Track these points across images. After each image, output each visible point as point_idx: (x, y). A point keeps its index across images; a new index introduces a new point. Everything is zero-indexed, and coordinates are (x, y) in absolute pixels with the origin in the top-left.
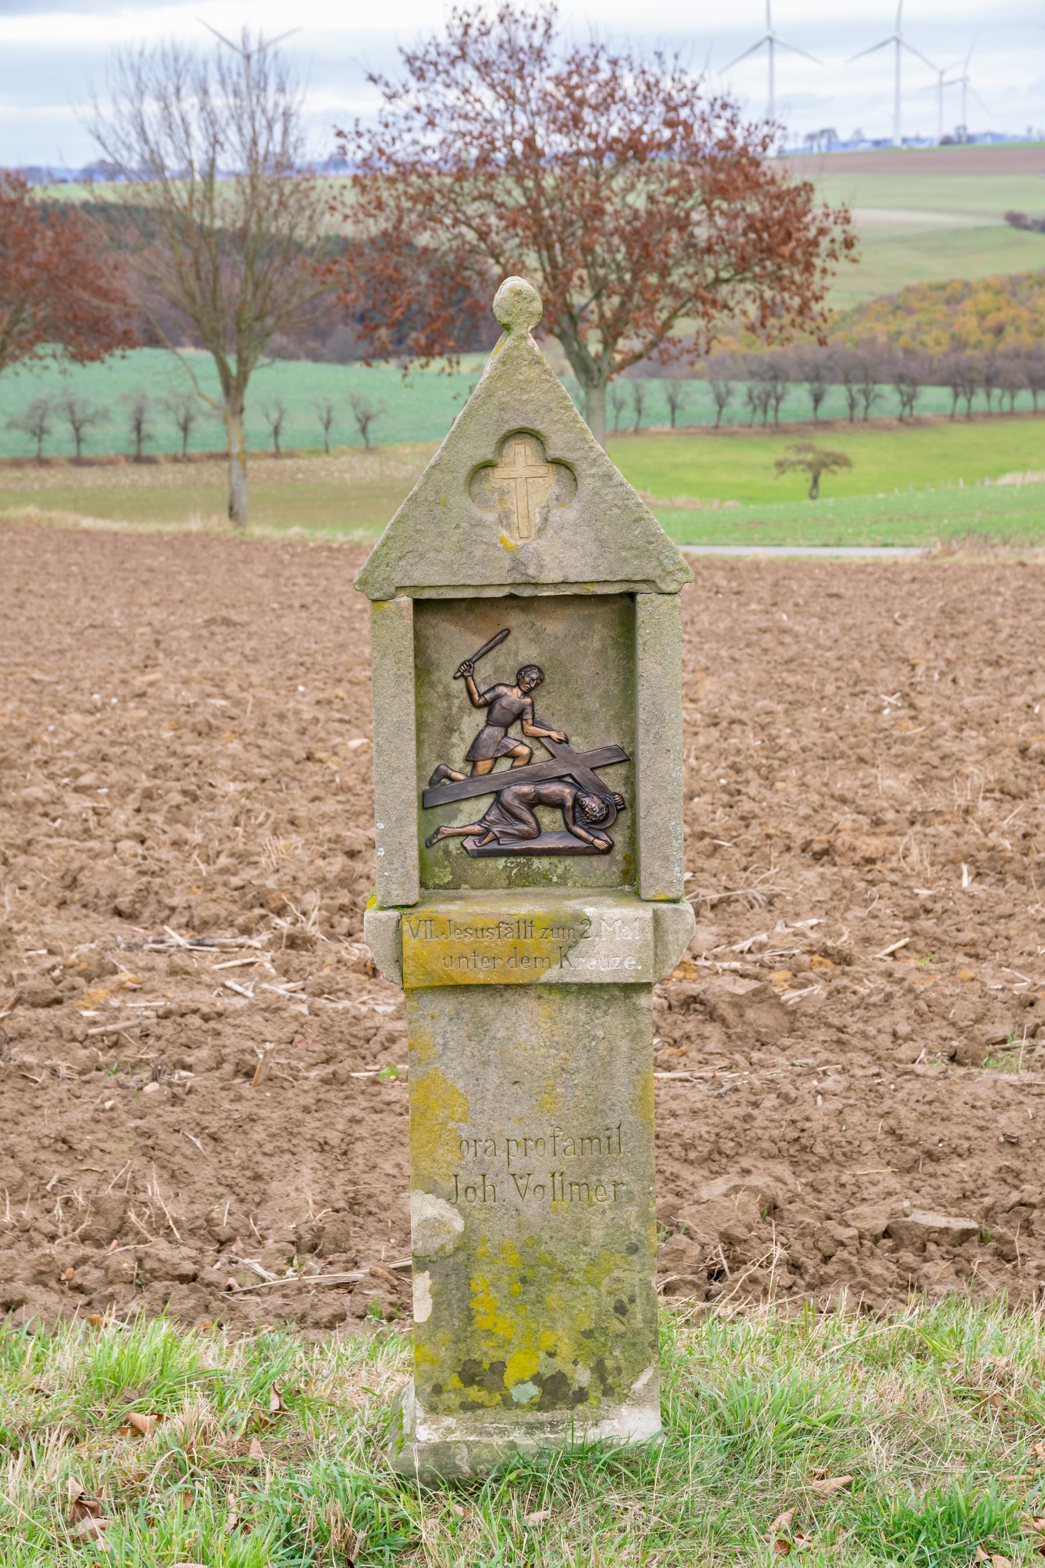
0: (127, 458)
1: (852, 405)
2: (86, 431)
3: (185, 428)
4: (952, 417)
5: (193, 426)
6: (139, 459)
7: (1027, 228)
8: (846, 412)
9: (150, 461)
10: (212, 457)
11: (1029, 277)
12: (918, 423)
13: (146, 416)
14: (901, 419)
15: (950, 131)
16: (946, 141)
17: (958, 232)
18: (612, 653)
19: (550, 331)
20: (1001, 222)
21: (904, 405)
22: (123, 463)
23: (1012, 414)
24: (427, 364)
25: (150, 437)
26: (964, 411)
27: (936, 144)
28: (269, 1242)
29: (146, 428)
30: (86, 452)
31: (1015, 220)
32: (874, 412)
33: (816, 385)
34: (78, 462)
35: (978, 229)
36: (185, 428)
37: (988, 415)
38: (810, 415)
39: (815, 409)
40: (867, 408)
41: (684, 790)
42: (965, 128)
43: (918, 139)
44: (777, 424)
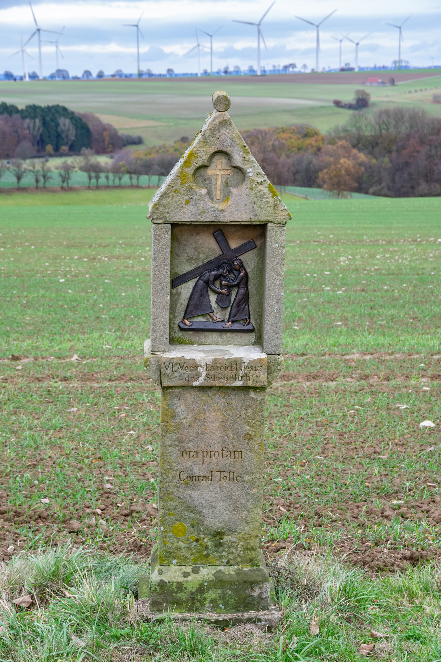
1: (37, 181)
4: (89, 188)
7: (342, 107)
8: (34, 184)
12: (71, 189)
14: (62, 188)
15: (343, 65)
16: (342, 70)
17: (312, 108)
20: (332, 104)
21: (63, 182)
23: (120, 187)
26: (95, 185)
27: (338, 70)
28: (5, 474)
31: (337, 104)
32: (47, 185)
33: (107, 174)
35: (321, 107)
37: (107, 187)
38: (16, 185)
39: (18, 183)
40: (45, 183)
42: (349, 64)
43: (187, 74)
44: (44, 187)
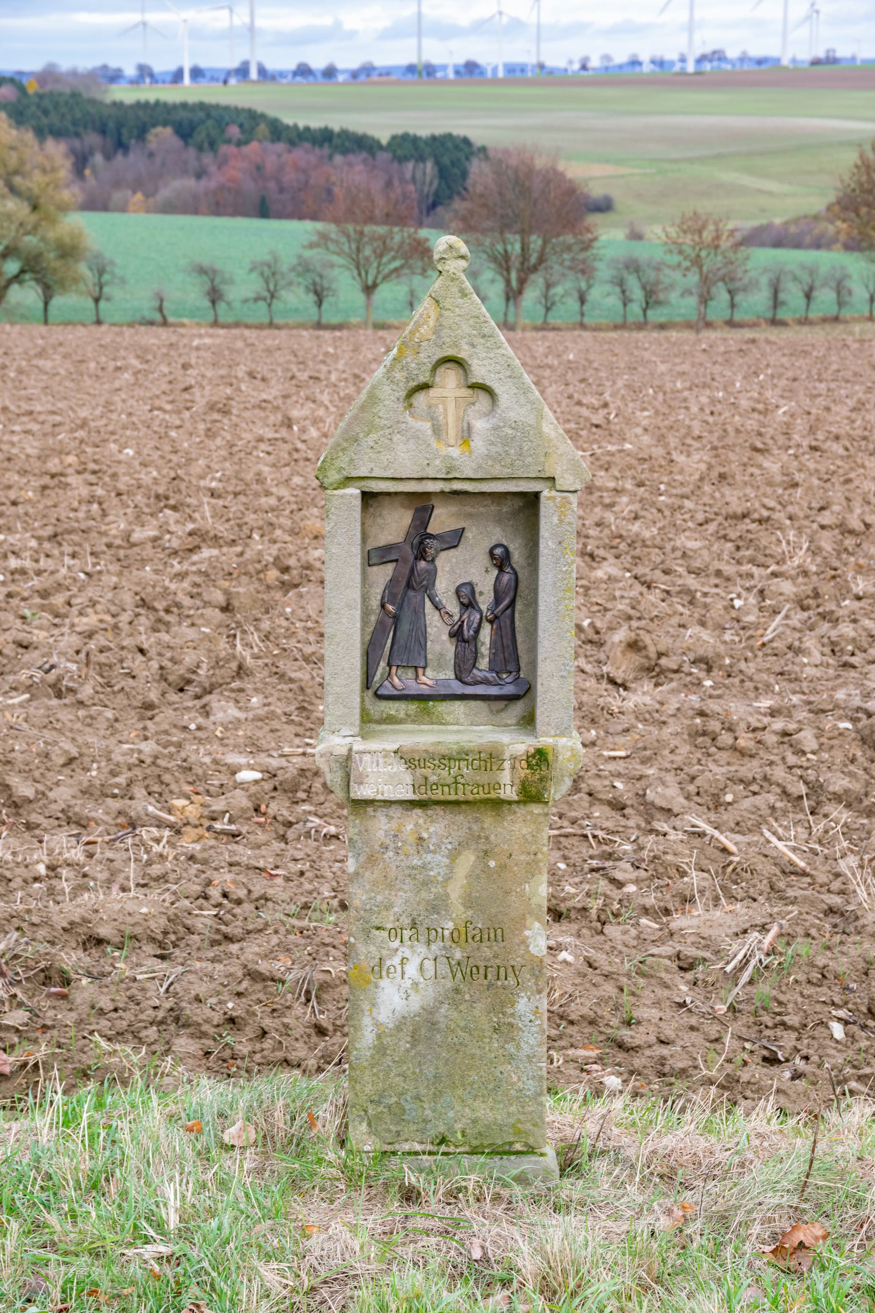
0: (766, 320)
2: (738, 298)
3: (808, 296)
5: (815, 294)
6: (774, 322)
9: (783, 324)
10: (824, 320)
11: (806, 217)
13: (782, 286)
15: (821, 54)
16: (816, 62)
18: (430, 812)
19: (299, 264)
22: (764, 326)
24: (229, 304)
25: (783, 303)
29: (782, 296)
30: (737, 317)
34: (731, 324)
36: (808, 296)
41: (442, 1129)
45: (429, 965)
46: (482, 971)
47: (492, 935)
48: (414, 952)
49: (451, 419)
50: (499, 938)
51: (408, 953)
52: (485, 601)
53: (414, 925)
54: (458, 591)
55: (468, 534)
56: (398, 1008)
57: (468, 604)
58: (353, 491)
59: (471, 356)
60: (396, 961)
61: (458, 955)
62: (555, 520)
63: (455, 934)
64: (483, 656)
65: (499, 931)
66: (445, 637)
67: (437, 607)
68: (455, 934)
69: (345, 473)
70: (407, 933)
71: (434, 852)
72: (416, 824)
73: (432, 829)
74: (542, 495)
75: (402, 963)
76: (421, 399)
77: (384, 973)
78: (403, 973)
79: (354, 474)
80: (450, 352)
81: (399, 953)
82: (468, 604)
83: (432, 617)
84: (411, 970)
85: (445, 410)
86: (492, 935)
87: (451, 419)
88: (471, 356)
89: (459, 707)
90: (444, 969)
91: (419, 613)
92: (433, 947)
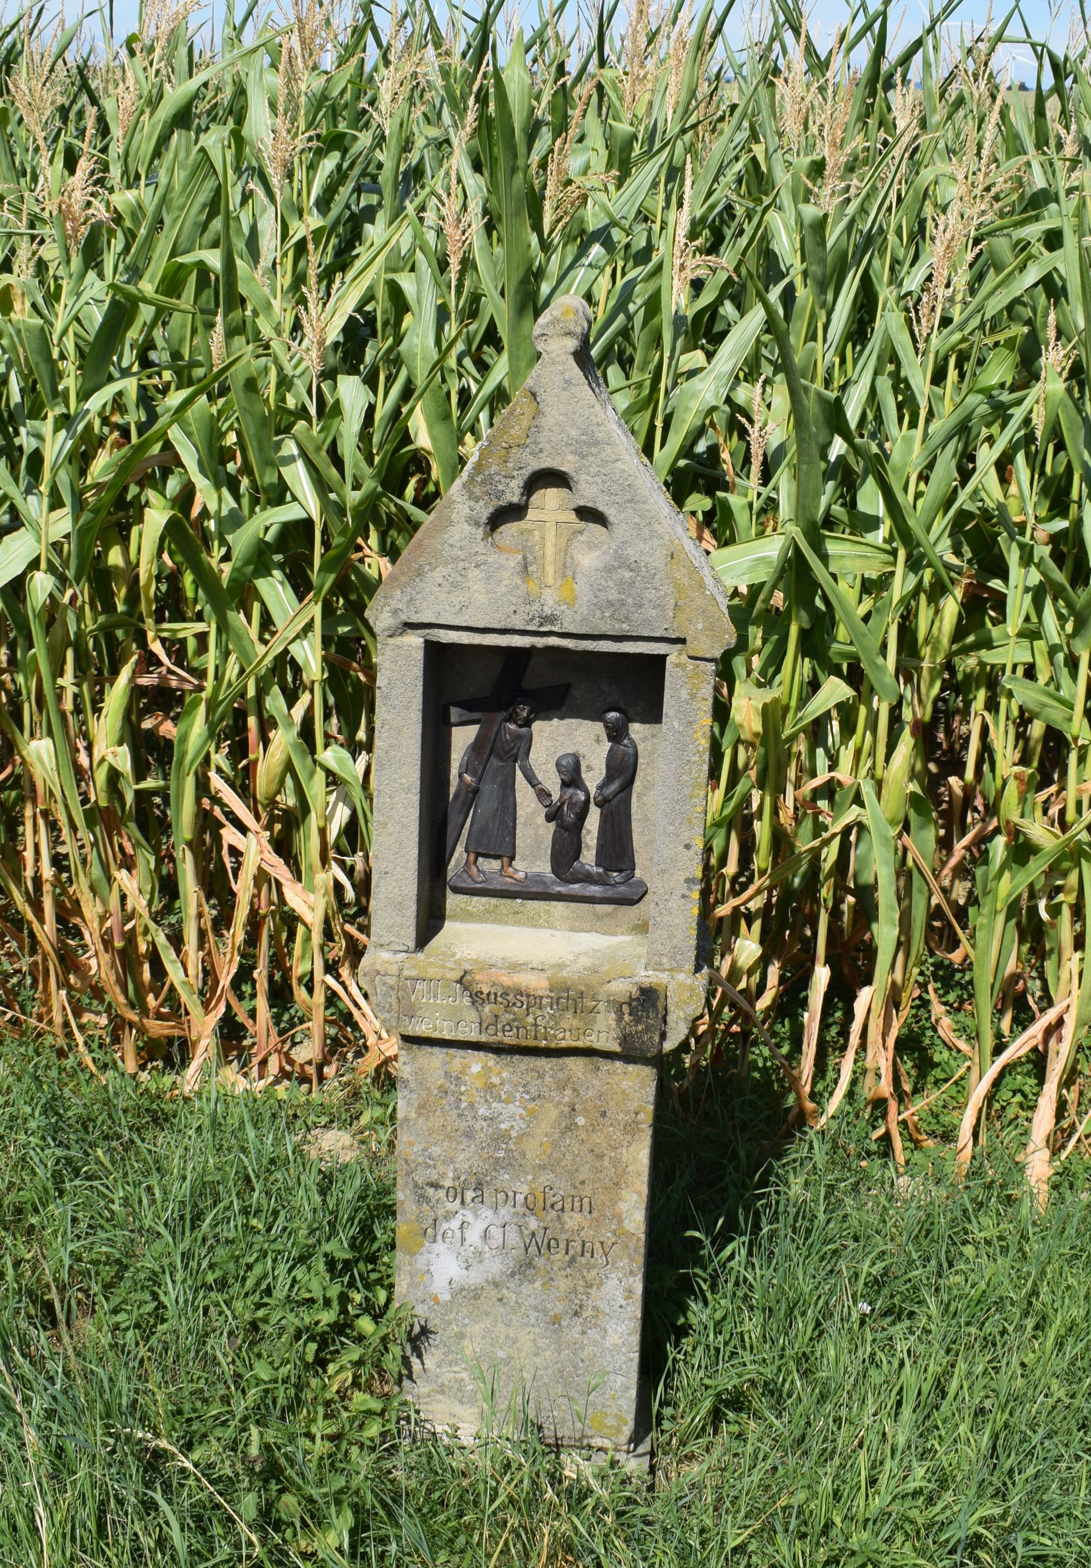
45: (496, 1232)
46: (563, 1245)
47: (577, 1205)
48: (477, 1216)
49: (550, 551)
50: (586, 1207)
51: (470, 1217)
52: (593, 777)
53: (479, 1186)
54: (558, 764)
55: (576, 692)
56: (456, 1278)
57: (572, 777)
58: (415, 641)
59: (578, 470)
60: (455, 1224)
61: (533, 1224)
62: (684, 694)
63: (530, 1199)
64: (588, 848)
65: (586, 1200)
66: (541, 819)
67: (531, 779)
68: (530, 1199)
69: (404, 617)
70: (469, 1195)
71: (507, 1102)
72: (485, 1067)
73: (505, 1075)
74: (668, 659)
75: (462, 1227)
76: (509, 530)
77: (439, 1238)
78: (463, 1239)
79: (415, 619)
80: (546, 463)
81: (459, 1216)
82: (572, 777)
83: (524, 792)
84: (474, 1236)
85: (543, 538)
86: (577, 1205)
87: (550, 551)
88: (578, 470)
89: (558, 907)
90: (513, 1238)
91: (509, 787)
92: (503, 1211)
